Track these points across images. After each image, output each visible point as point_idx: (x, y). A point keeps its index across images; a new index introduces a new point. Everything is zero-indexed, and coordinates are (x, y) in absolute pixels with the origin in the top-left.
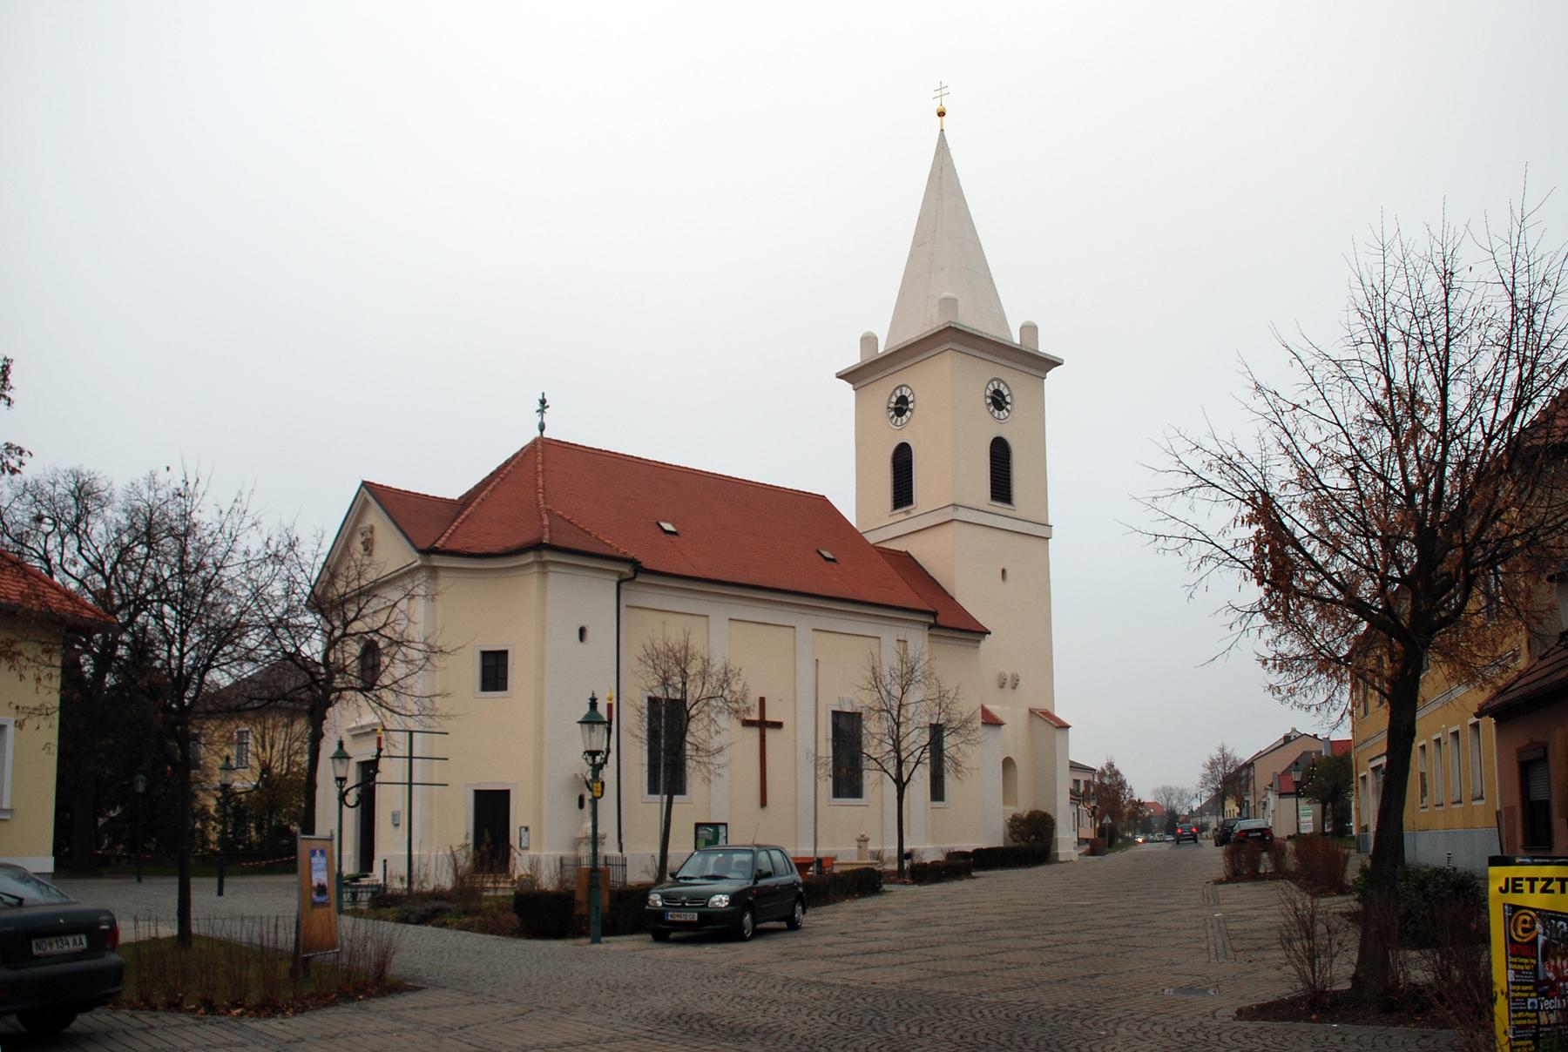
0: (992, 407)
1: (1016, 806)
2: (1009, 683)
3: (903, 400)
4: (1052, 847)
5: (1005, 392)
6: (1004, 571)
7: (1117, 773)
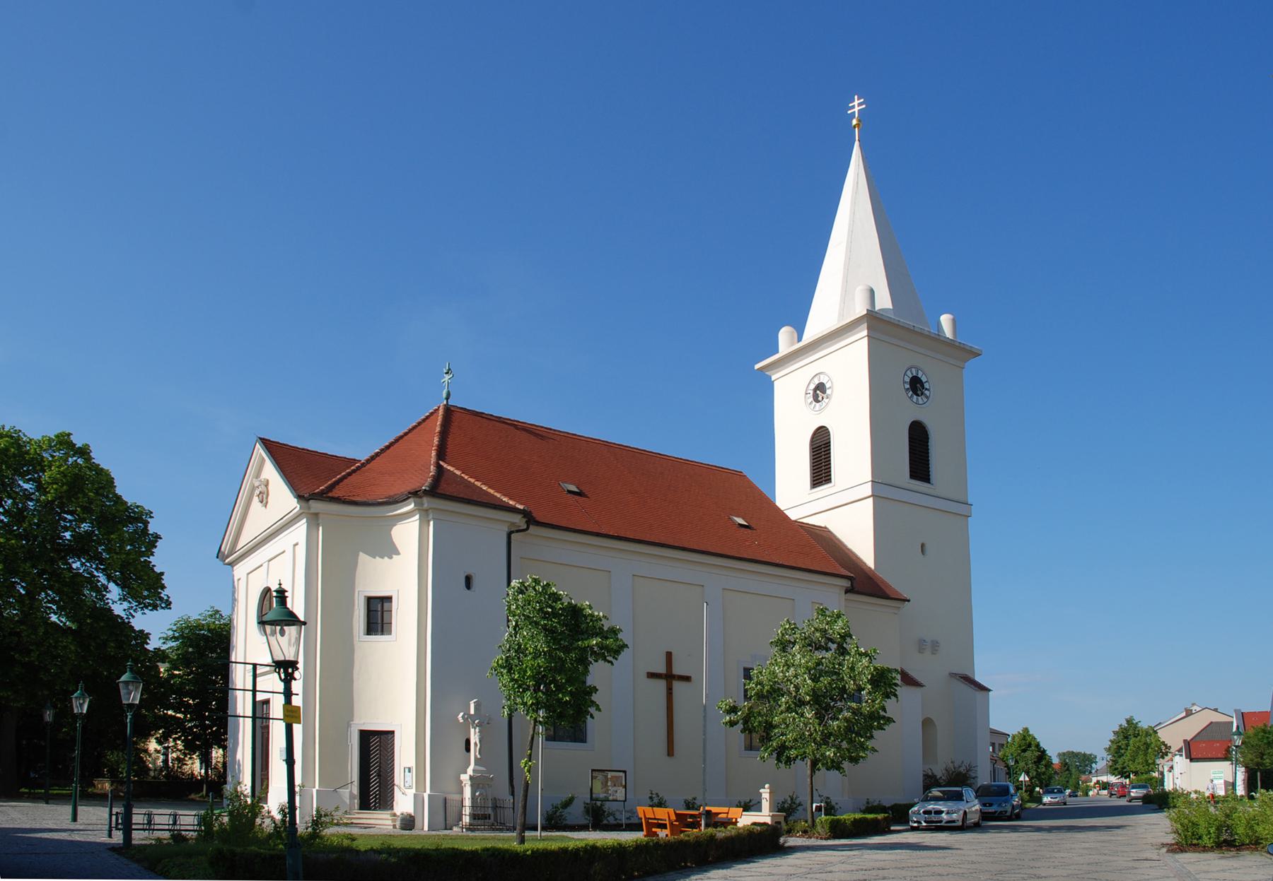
0: (911, 392)
2: (928, 646)
3: (821, 388)
5: (924, 379)
6: (923, 545)
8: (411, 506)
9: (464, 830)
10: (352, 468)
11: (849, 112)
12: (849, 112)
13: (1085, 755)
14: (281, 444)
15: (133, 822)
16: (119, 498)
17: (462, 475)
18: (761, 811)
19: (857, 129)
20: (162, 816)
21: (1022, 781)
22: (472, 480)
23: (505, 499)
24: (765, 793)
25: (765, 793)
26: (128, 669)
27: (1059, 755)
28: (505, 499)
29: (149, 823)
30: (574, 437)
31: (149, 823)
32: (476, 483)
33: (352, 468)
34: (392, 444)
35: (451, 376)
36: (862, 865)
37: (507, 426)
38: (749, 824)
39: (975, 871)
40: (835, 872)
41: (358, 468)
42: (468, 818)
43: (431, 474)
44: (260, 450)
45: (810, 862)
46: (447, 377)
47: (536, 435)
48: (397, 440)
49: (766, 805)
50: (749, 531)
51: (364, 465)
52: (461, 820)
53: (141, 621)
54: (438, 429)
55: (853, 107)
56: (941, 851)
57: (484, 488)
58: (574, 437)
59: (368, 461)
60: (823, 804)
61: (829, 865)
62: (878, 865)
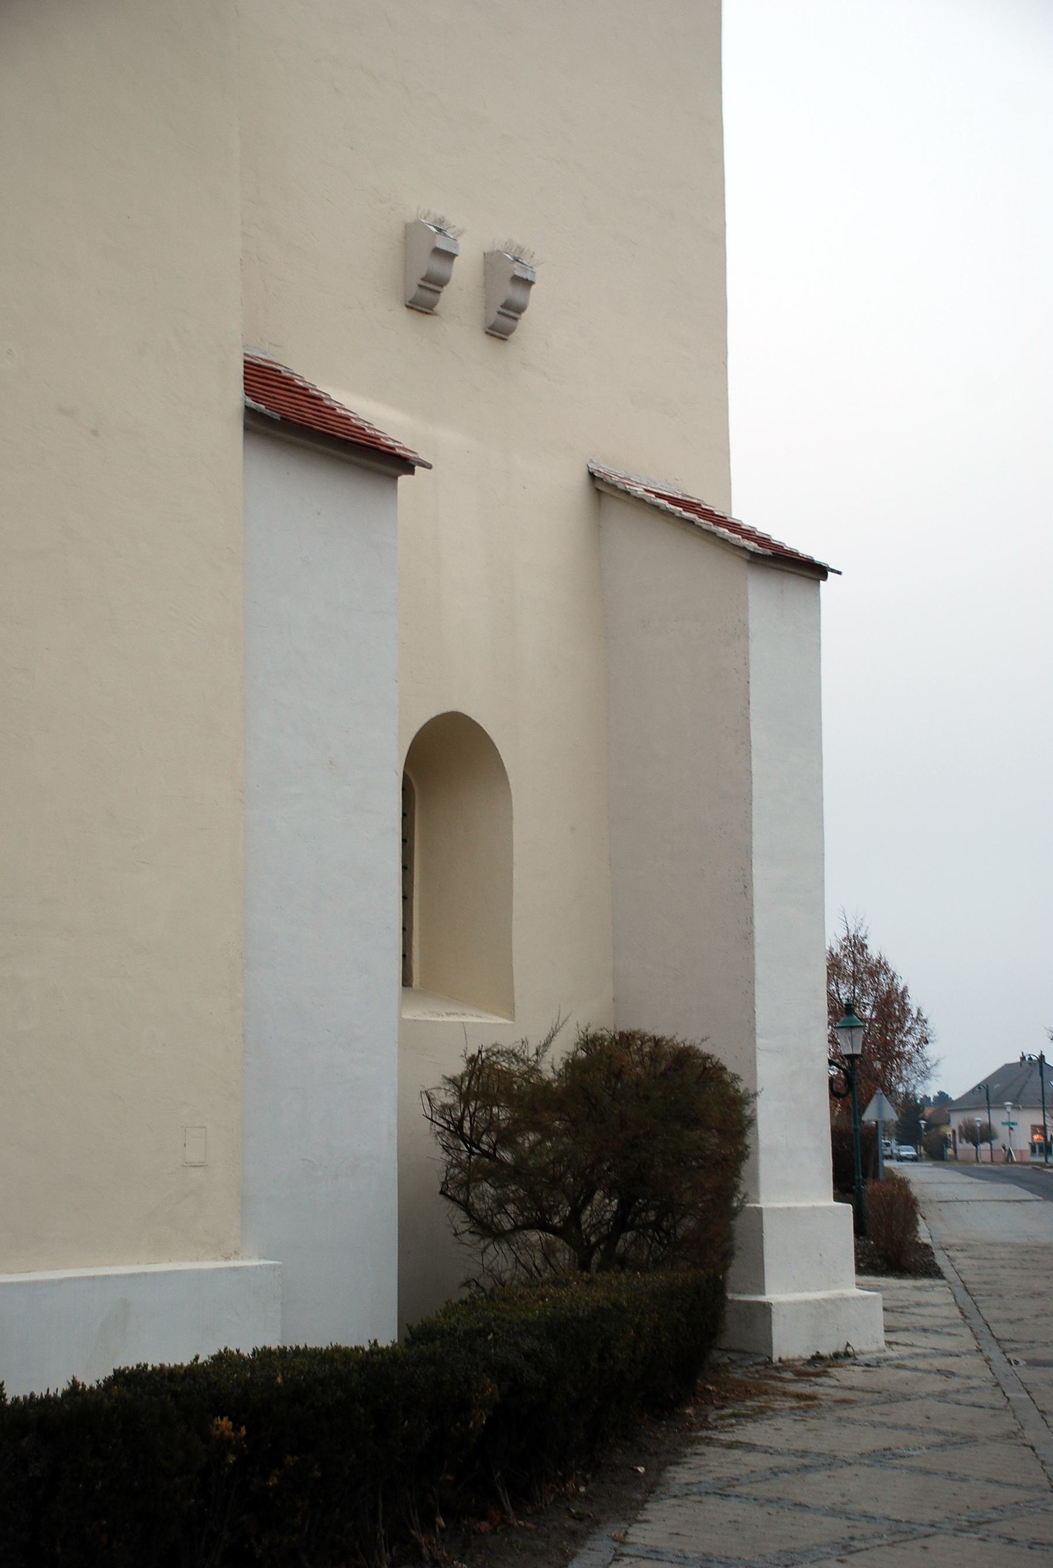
1: (508, 1008)
4: (735, 1272)
7: (878, 969)
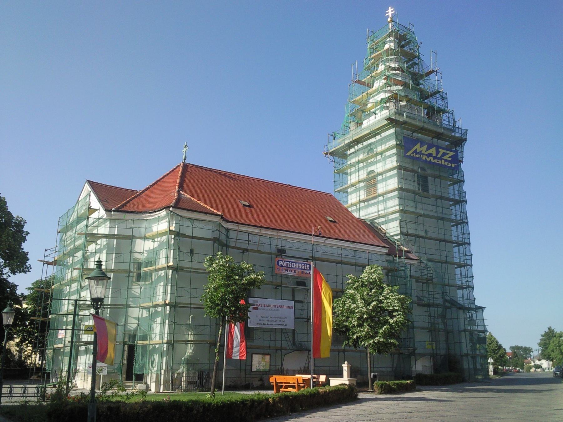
8: (163, 213)
9: (182, 391)
10: (135, 195)
11: (386, 15)
12: (386, 15)
13: (526, 347)
14: (99, 183)
15: (2, 392)
16: (10, 213)
17: (191, 198)
18: (343, 377)
19: (390, 23)
20: (18, 389)
21: (489, 362)
22: (196, 200)
23: (212, 210)
24: (345, 367)
25: (345, 366)
26: (8, 305)
27: (512, 348)
28: (212, 210)
29: (10, 393)
30: (247, 178)
31: (10, 393)
32: (198, 202)
33: (135, 195)
34: (156, 183)
35: (187, 148)
36: (399, 410)
37: (214, 173)
38: (338, 384)
39: (462, 414)
40: (384, 414)
41: (138, 195)
42: (185, 384)
43: (175, 197)
44: (87, 188)
45: (370, 408)
46: (185, 149)
47: (229, 177)
48: (158, 181)
49: (345, 374)
50: (335, 224)
51: (141, 193)
52: (181, 385)
53: (13, 279)
54: (180, 175)
55: (392, 11)
56: (443, 402)
57: (202, 204)
58: (247, 178)
59: (143, 192)
60: (377, 374)
61: (380, 409)
62: (407, 410)
